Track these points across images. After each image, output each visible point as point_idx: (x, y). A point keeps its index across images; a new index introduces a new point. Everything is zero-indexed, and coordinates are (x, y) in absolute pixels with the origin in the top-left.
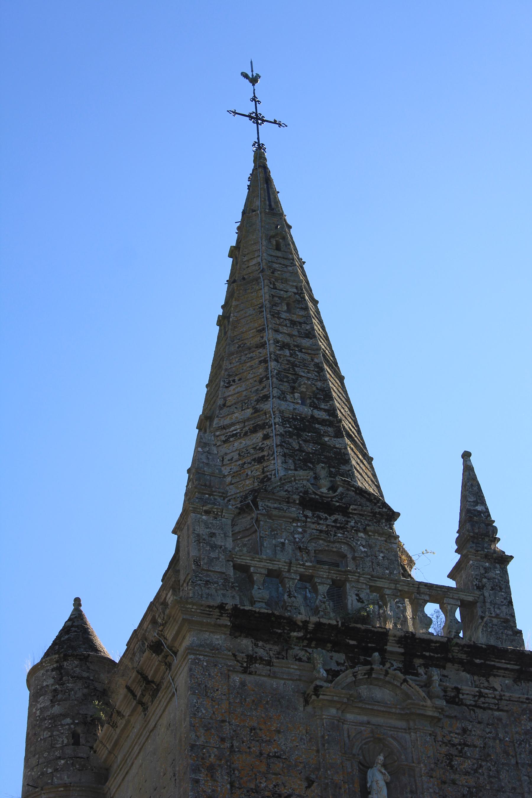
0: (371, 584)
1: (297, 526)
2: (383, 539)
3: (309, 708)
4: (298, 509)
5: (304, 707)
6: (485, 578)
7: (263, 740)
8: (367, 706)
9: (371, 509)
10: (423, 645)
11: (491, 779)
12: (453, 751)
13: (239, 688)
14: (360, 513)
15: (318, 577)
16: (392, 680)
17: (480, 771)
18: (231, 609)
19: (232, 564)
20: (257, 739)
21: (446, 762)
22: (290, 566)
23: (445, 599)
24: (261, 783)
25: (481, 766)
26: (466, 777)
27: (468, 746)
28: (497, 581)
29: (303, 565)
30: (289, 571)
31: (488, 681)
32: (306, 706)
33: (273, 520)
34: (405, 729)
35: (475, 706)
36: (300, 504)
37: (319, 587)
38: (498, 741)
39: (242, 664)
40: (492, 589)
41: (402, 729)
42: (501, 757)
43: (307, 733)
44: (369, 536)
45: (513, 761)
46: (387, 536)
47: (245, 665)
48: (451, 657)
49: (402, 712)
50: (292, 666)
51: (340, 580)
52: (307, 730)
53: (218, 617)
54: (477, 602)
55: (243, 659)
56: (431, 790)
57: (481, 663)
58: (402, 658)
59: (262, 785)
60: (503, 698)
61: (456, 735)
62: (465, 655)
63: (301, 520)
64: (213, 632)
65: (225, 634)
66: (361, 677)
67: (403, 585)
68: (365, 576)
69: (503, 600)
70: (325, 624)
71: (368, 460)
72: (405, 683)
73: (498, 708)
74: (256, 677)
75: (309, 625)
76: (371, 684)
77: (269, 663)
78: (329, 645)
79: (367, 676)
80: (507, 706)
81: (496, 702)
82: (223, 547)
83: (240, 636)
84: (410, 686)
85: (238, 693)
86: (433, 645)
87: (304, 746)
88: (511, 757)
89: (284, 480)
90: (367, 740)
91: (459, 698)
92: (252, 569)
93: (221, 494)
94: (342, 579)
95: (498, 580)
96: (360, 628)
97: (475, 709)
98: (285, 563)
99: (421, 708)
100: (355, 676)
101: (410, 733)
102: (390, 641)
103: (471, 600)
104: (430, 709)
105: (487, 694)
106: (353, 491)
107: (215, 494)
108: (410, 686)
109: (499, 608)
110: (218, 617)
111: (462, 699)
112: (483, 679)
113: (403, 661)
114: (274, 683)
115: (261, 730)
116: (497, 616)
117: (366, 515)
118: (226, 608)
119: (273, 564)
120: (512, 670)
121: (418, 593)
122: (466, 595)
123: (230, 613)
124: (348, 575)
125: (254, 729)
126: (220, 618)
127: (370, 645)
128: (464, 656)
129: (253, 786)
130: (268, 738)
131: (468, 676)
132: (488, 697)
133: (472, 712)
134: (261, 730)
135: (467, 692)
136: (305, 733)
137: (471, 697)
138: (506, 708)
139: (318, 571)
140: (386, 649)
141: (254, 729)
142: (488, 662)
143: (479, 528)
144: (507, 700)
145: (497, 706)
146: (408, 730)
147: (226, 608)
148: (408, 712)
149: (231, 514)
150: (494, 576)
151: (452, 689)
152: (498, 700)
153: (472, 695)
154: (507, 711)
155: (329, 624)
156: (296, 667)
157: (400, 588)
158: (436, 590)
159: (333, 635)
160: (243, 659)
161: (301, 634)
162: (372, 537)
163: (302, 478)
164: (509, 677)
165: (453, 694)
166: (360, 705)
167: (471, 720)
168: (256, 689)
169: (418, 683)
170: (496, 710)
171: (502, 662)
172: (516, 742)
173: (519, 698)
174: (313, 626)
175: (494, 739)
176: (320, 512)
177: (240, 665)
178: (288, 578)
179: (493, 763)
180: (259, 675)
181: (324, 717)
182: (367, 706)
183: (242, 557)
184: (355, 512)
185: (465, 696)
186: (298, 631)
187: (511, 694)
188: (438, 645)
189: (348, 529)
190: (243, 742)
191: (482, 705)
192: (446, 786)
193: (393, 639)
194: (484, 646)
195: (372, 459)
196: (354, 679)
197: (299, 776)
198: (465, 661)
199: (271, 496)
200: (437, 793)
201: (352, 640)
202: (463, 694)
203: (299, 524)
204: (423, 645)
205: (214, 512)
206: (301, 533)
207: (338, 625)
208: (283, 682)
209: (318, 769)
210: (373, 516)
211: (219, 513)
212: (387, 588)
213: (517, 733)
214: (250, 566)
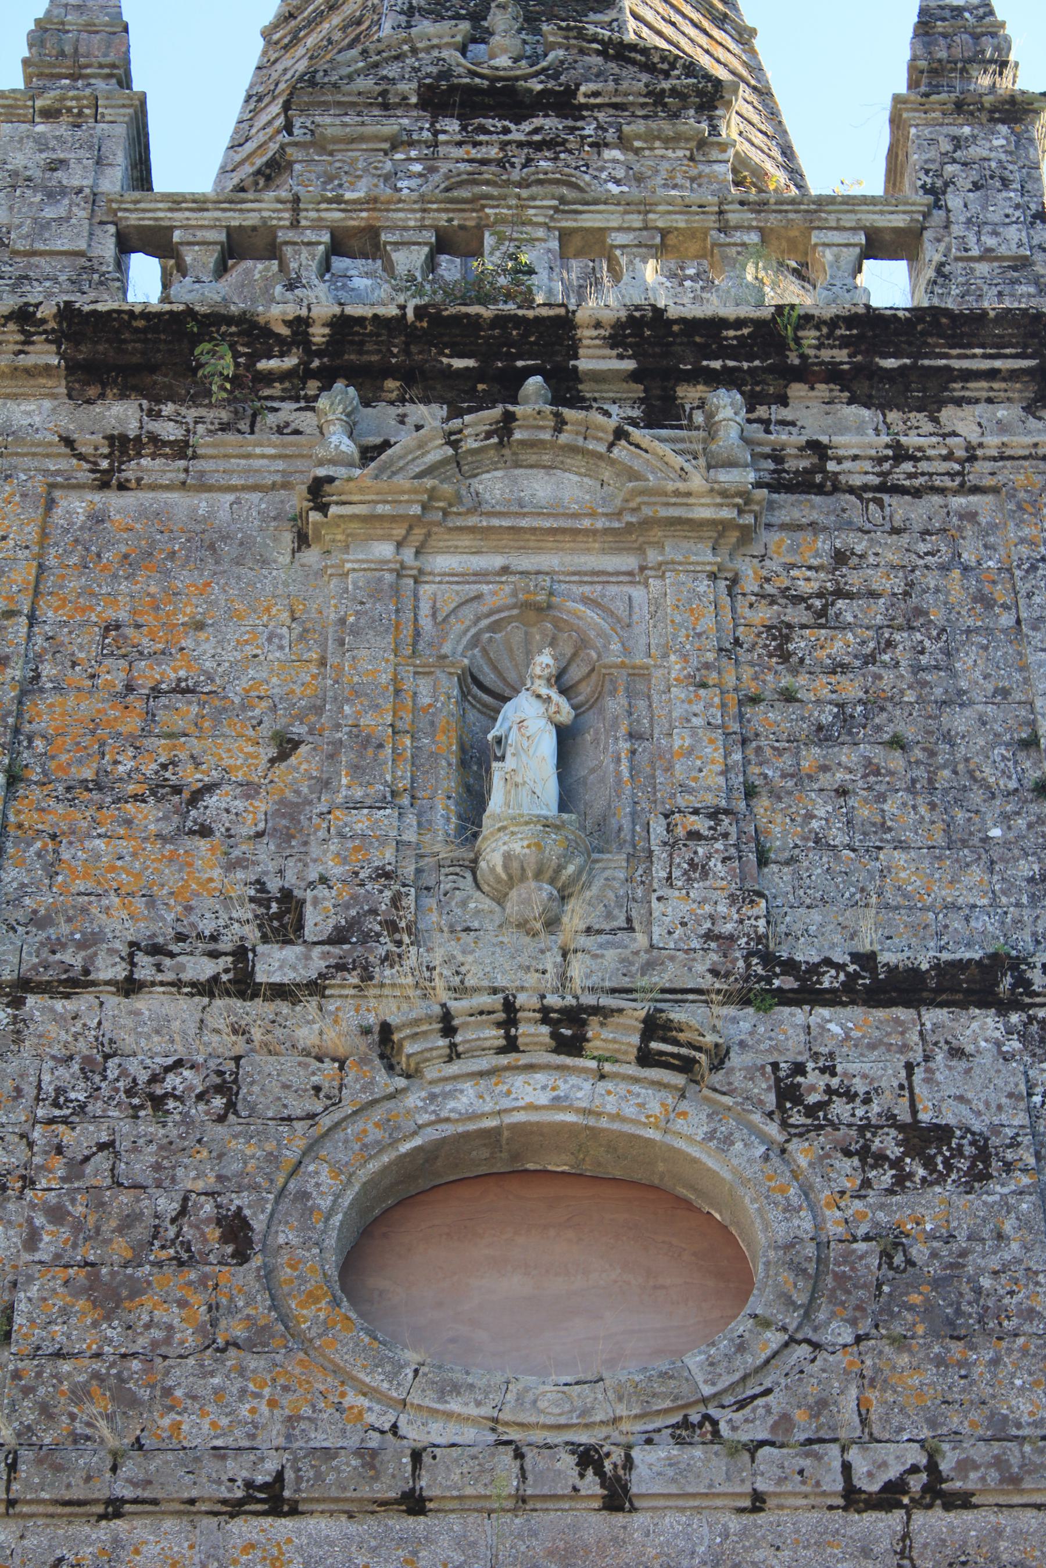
0: (564, 224)
1: (409, 159)
2: (680, 153)
3: (311, 556)
4: (418, 119)
5: (293, 552)
6: (954, 161)
7: (141, 653)
8: (496, 522)
9: (647, 86)
10: (698, 339)
11: (922, 675)
12: (796, 615)
13: (81, 528)
14: (614, 100)
15: (391, 229)
16: (581, 439)
17: (886, 657)
18: (55, 316)
19: (112, 229)
20: (123, 651)
21: (766, 646)
22: (296, 211)
23: (815, 233)
24: (116, 762)
25: (890, 644)
26: (833, 679)
27: (849, 596)
28: (993, 164)
29: (338, 200)
30: (295, 224)
31: (936, 420)
32: (299, 549)
33: (331, 154)
34: (630, 574)
35: (882, 488)
36: (424, 104)
37: (395, 256)
38: (956, 573)
39: (95, 464)
40: (976, 187)
41: (618, 574)
42: (964, 613)
43: (294, 619)
44: (637, 151)
45: (1006, 620)
46: (693, 144)
47: (105, 464)
48: (797, 362)
49: (616, 525)
50: (258, 451)
51: (462, 227)
52: (292, 612)
53: (19, 347)
54: (924, 228)
55: (96, 449)
56: (696, 721)
57: (903, 368)
58: (638, 390)
59: (121, 768)
60: (979, 452)
61: (809, 573)
62: (845, 352)
63: (419, 142)
64: (14, 397)
65: (54, 396)
66: (476, 445)
67: (669, 213)
68: (538, 203)
69: (1010, 211)
70: (361, 320)
71: (740, 35)
72: (623, 442)
73: (962, 485)
74: (140, 494)
75: (311, 330)
76: (517, 465)
77: (182, 449)
78: (391, 384)
79: (495, 440)
80: (992, 474)
81: (957, 467)
82: (87, 191)
83: (102, 396)
84: (638, 446)
85: (76, 541)
86: (731, 333)
87: (278, 654)
88: (997, 610)
89: (379, 53)
90: (496, 617)
91: (823, 471)
92: (177, 236)
93: (107, 71)
94: (471, 223)
95: (1000, 161)
96: (479, 316)
97: (886, 498)
98: (280, 201)
99: (673, 500)
100: (455, 445)
101: (646, 585)
102: (586, 342)
103: (901, 225)
104: (703, 501)
105: (920, 449)
106: (599, 53)
107: (88, 71)
108: (638, 446)
109: (995, 233)
110: (19, 347)
111: (836, 474)
112: (919, 418)
113: (642, 400)
114: (202, 503)
115: (138, 626)
116: (987, 255)
117: (632, 104)
118: (39, 315)
119: (241, 210)
120: (1013, 375)
121: (720, 230)
122: (882, 213)
123: (53, 331)
124: (484, 207)
125: (118, 627)
126: (26, 348)
127: (520, 364)
128: (841, 355)
129: (88, 774)
130: (161, 646)
131: (866, 413)
132: (928, 459)
133: (872, 506)
134: (138, 626)
135: (855, 451)
136: (288, 621)
137: (867, 465)
138: (988, 482)
139: (388, 210)
140: (575, 368)
141: (118, 627)
142: (926, 362)
143: (949, 47)
144: (994, 459)
145: (958, 480)
146: (637, 576)
147: (39, 315)
148: (634, 520)
149: (124, 106)
150: (985, 153)
151: (801, 449)
152: (961, 462)
153: (871, 458)
154: (995, 490)
155: (376, 316)
156: (272, 451)
157: (660, 224)
158: (780, 211)
159: (395, 350)
160: (96, 449)
161: (290, 362)
162: (647, 153)
163: (435, 41)
164: (1009, 399)
165: (803, 464)
166: (472, 521)
167: (868, 526)
168: (138, 526)
169: (679, 446)
170: (956, 492)
171: (974, 356)
172: (1019, 567)
173: (1036, 445)
174: (327, 331)
175: (944, 568)
176: (486, 117)
177: (86, 466)
178: (295, 243)
179: (935, 633)
180: (153, 487)
181: (348, 566)
182: (496, 522)
183: (142, 205)
184: (598, 100)
185: (847, 465)
186: (282, 355)
187: (1005, 439)
188: (746, 331)
189: (569, 146)
190: (74, 664)
191: (907, 483)
192: (762, 707)
193: (595, 333)
194: (900, 314)
195: (753, 33)
196: (450, 451)
197: (251, 733)
198: (846, 367)
199: (330, 98)
200: (717, 727)
201: (461, 356)
202: (839, 460)
203: (413, 154)
204: (698, 339)
205: (69, 110)
206: (420, 175)
207: (404, 315)
208: (230, 497)
209: (319, 710)
210: (655, 104)
211: (87, 111)
212: (619, 229)
213: (1022, 541)
214: (171, 229)
